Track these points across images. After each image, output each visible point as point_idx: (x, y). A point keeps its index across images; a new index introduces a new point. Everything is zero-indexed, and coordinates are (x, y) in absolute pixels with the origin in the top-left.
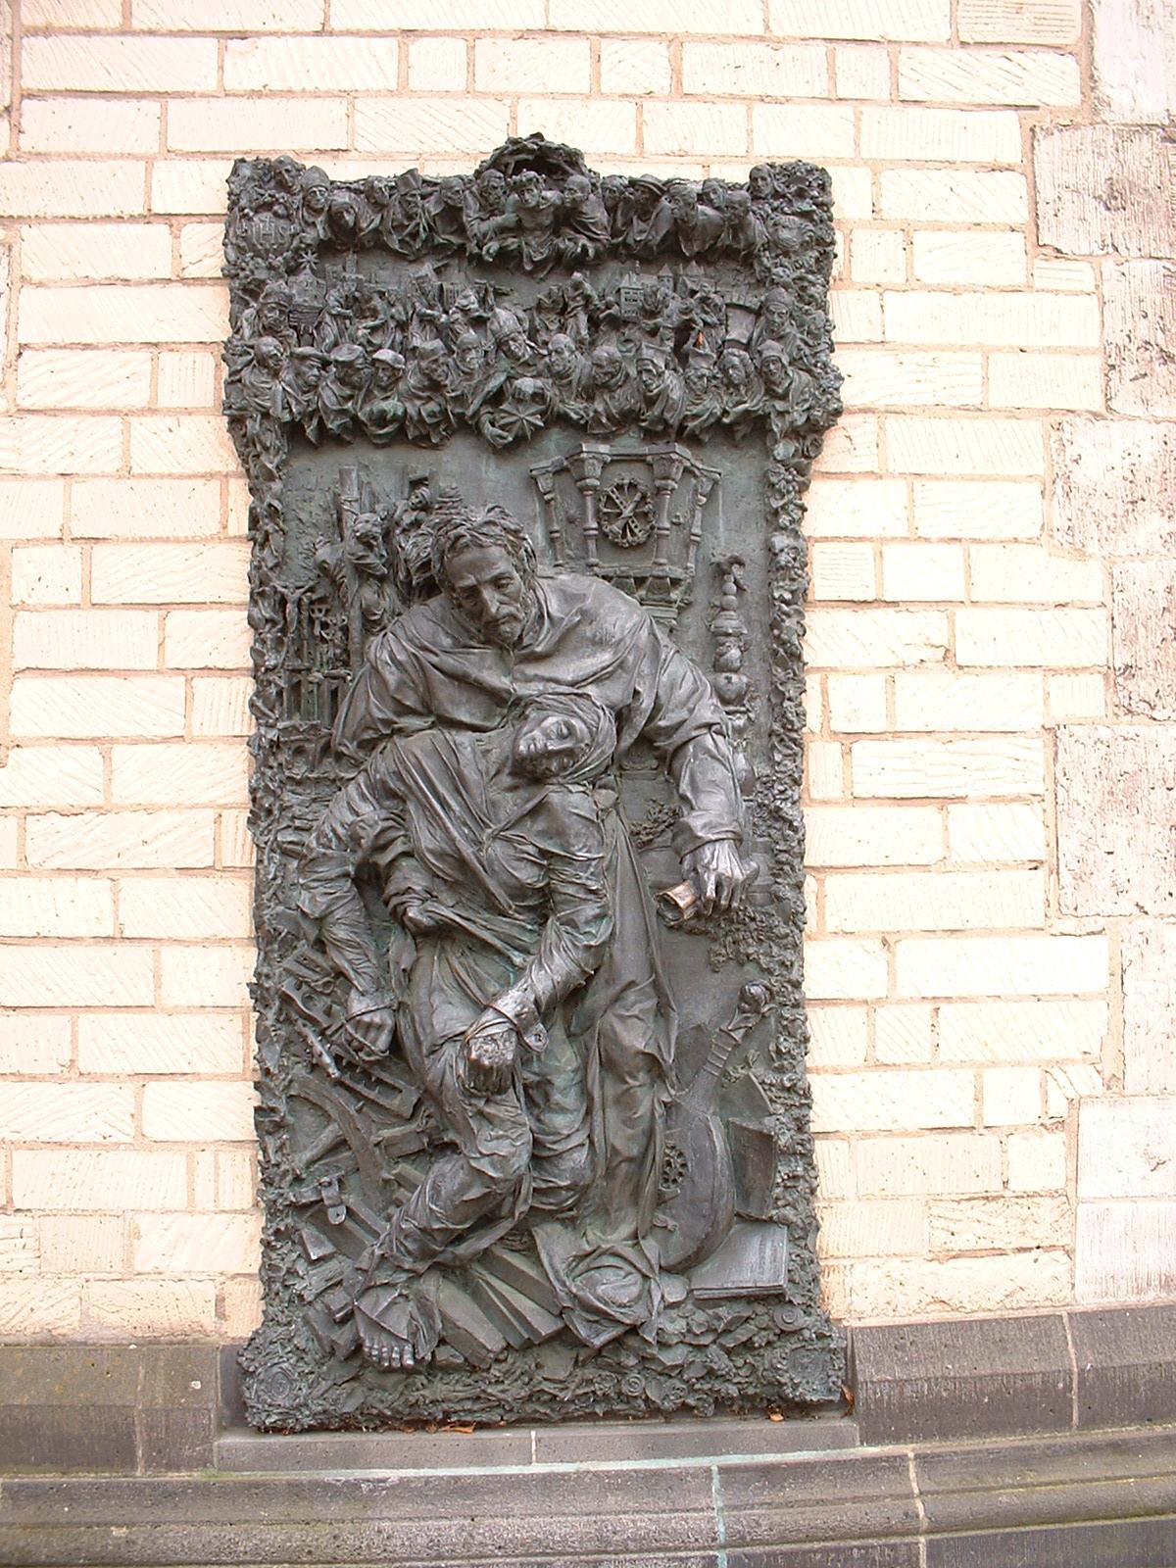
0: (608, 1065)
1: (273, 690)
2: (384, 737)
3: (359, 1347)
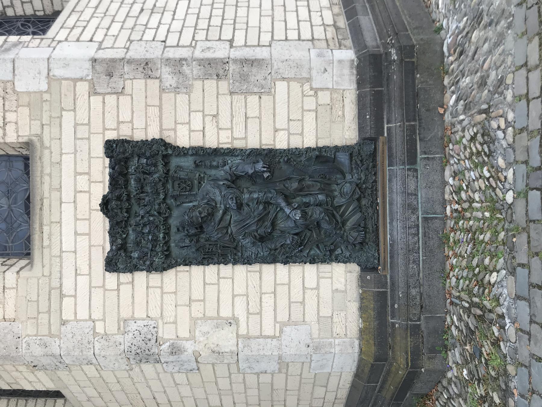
0: (301, 190)
1: (223, 260)
2: (233, 237)
3: (361, 243)
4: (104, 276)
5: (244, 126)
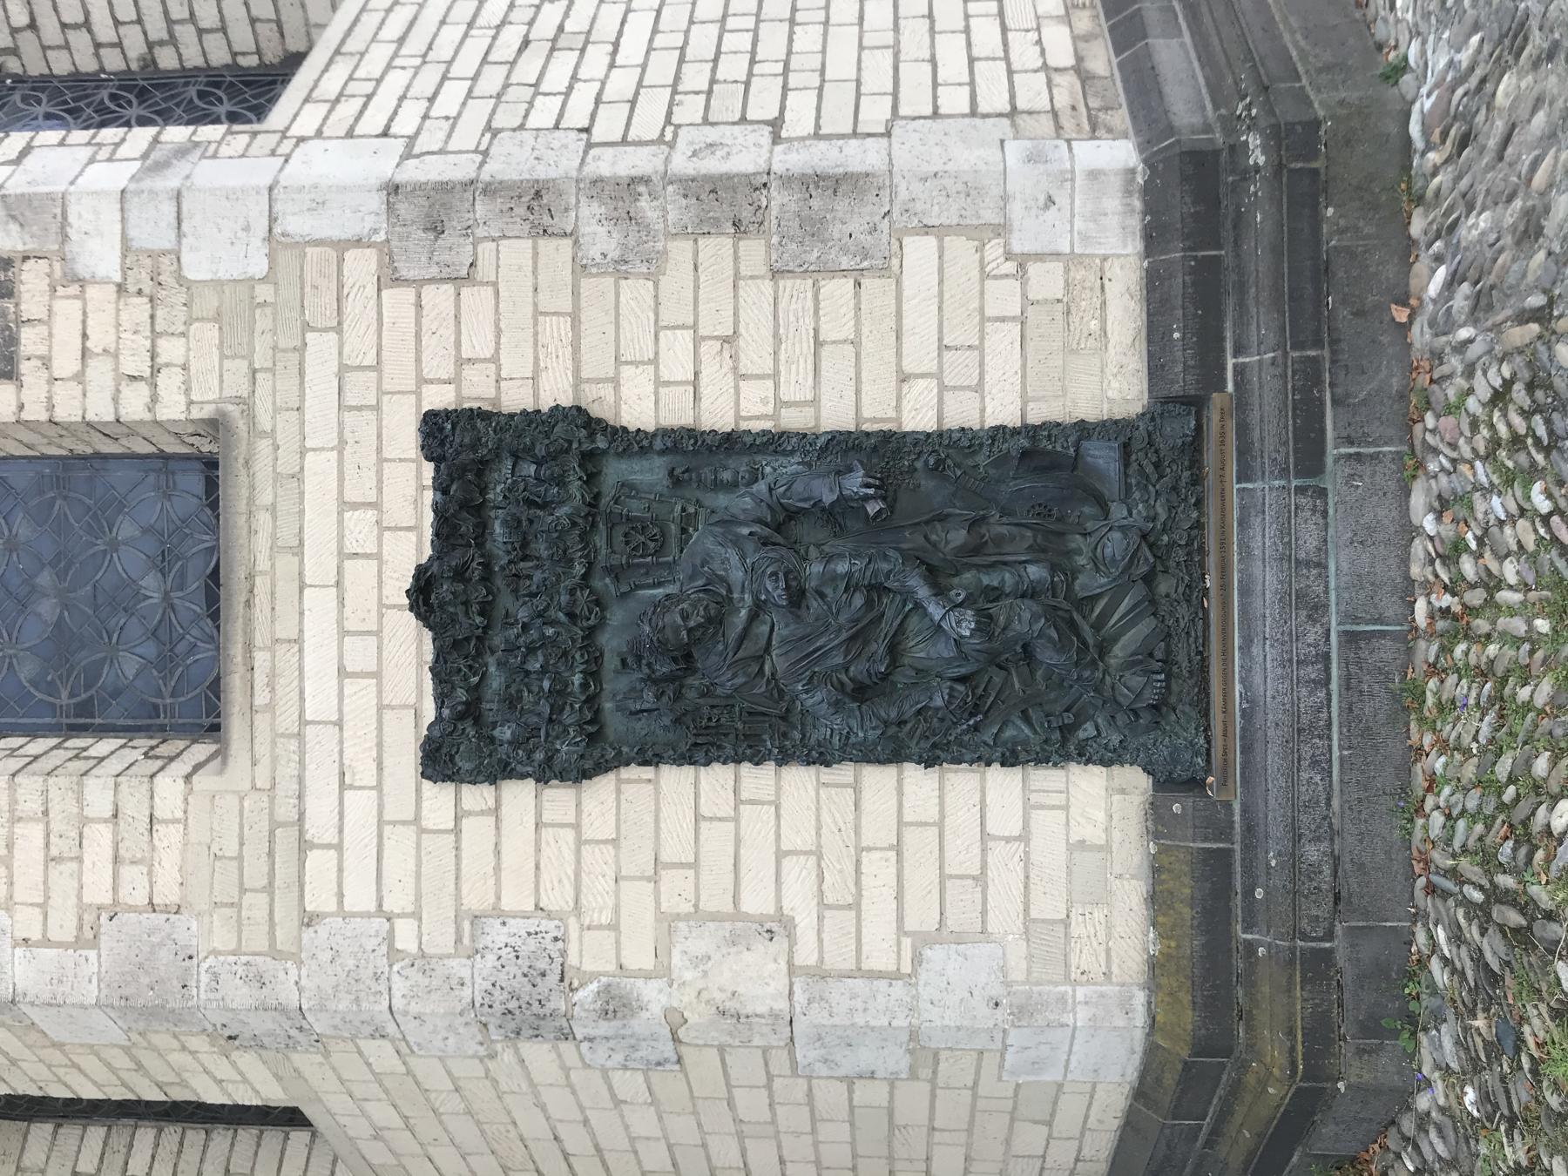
1: (748, 752)
2: (777, 685)
4: (418, 791)
5: (810, 367)
